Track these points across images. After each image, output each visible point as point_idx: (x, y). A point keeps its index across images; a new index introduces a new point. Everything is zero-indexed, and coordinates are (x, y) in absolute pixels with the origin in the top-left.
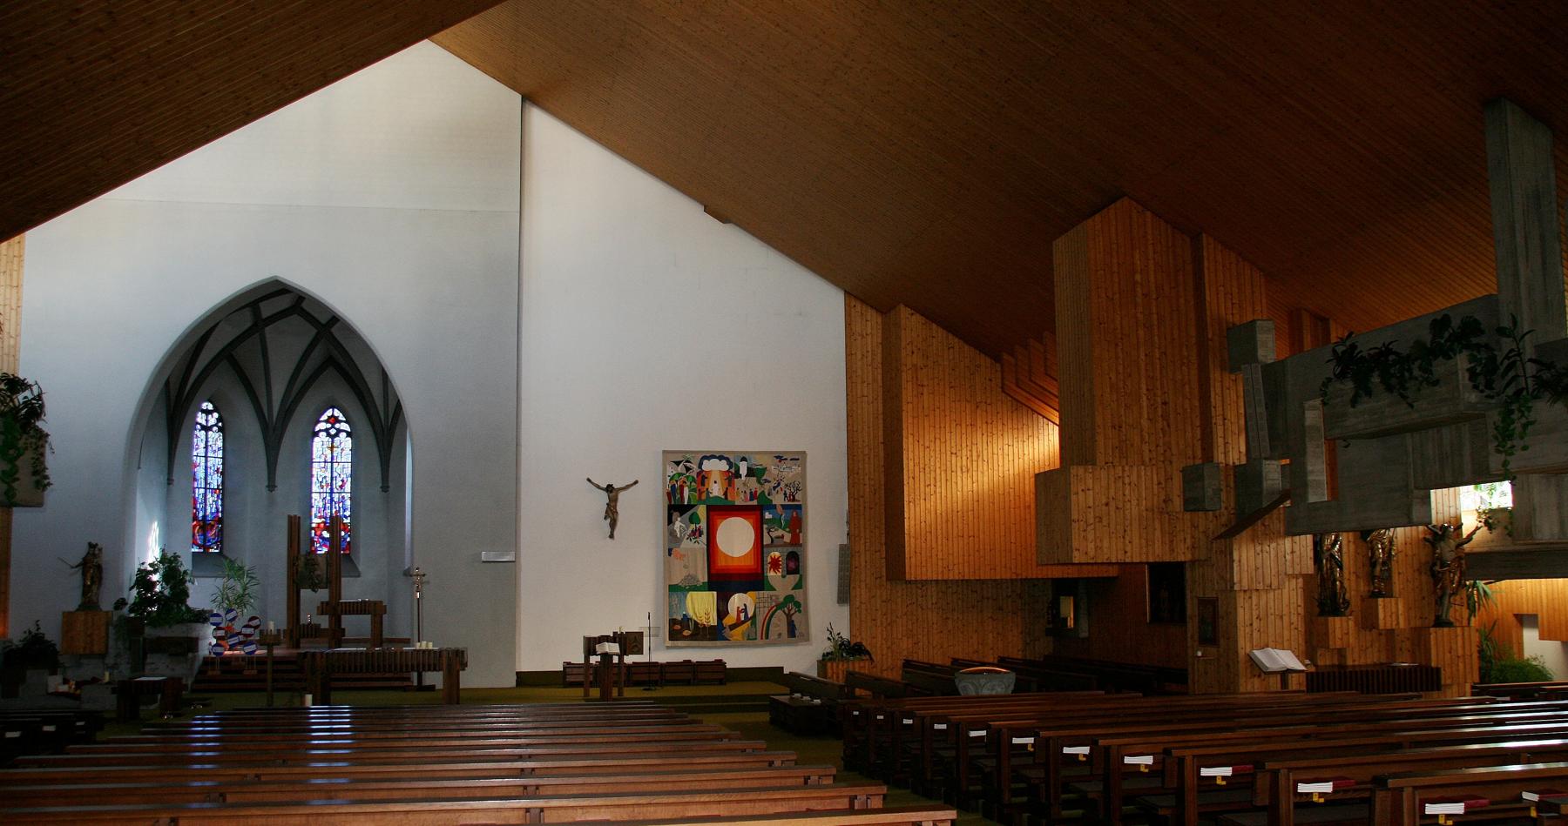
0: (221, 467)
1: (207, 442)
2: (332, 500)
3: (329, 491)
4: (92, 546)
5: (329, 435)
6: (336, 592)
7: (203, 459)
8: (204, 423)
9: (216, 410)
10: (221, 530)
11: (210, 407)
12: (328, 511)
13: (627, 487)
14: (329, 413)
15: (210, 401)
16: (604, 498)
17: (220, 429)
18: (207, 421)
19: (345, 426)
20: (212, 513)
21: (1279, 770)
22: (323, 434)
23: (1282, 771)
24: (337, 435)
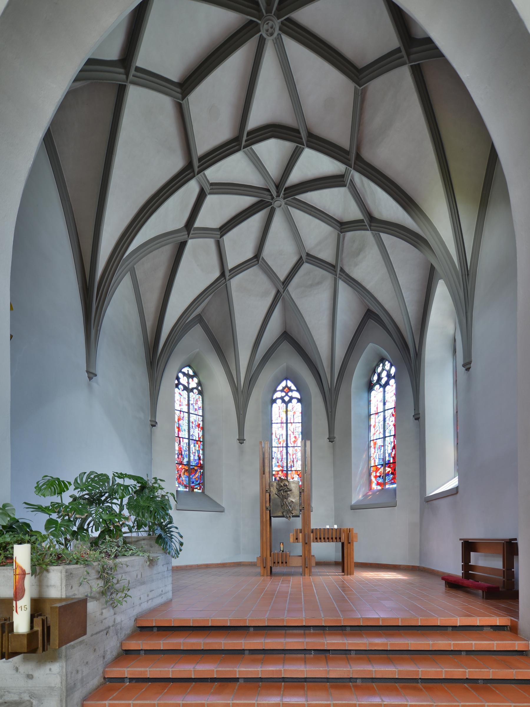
0: (201, 423)
1: (189, 401)
2: (287, 453)
3: (285, 445)
5: (283, 401)
6: (306, 521)
7: (186, 415)
8: (186, 385)
11: (191, 373)
12: (285, 461)
14: (283, 384)
15: (190, 366)
17: (201, 393)
18: (188, 383)
19: (296, 395)
20: (195, 460)
22: (279, 401)
24: (290, 401)
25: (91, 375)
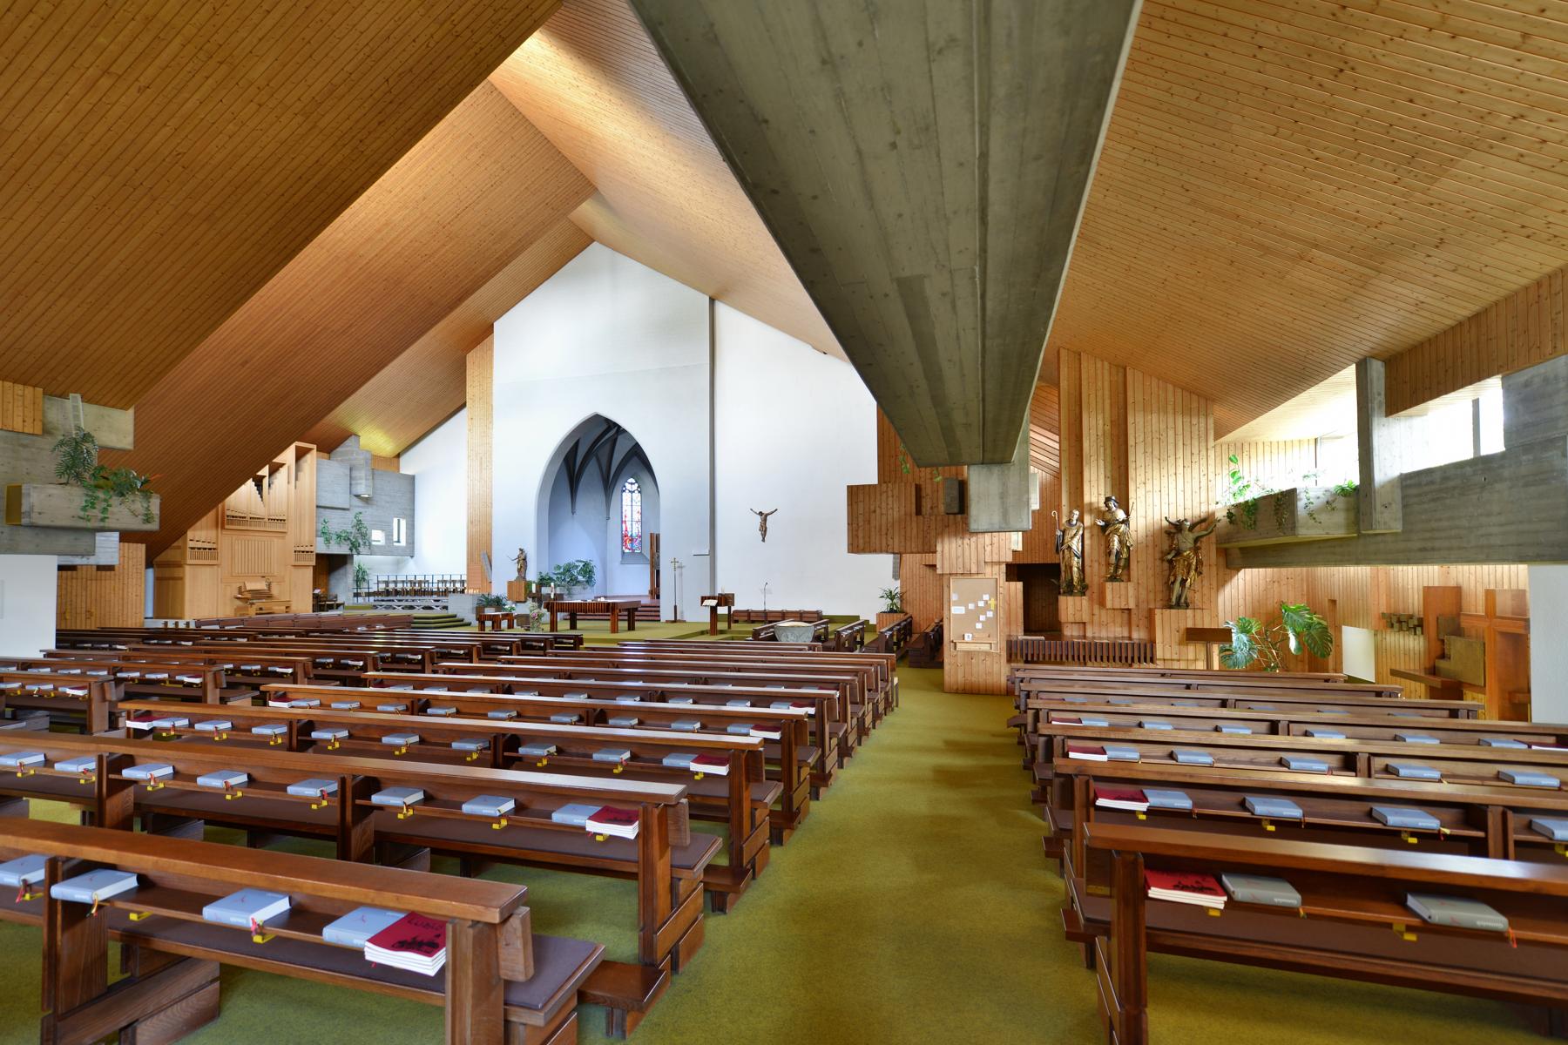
4: (521, 550)
9: (637, 482)
10: (641, 541)
13: (772, 513)
16: (758, 519)
17: (639, 492)
21: (1055, 736)
23: (1058, 737)
25: (573, 513)
